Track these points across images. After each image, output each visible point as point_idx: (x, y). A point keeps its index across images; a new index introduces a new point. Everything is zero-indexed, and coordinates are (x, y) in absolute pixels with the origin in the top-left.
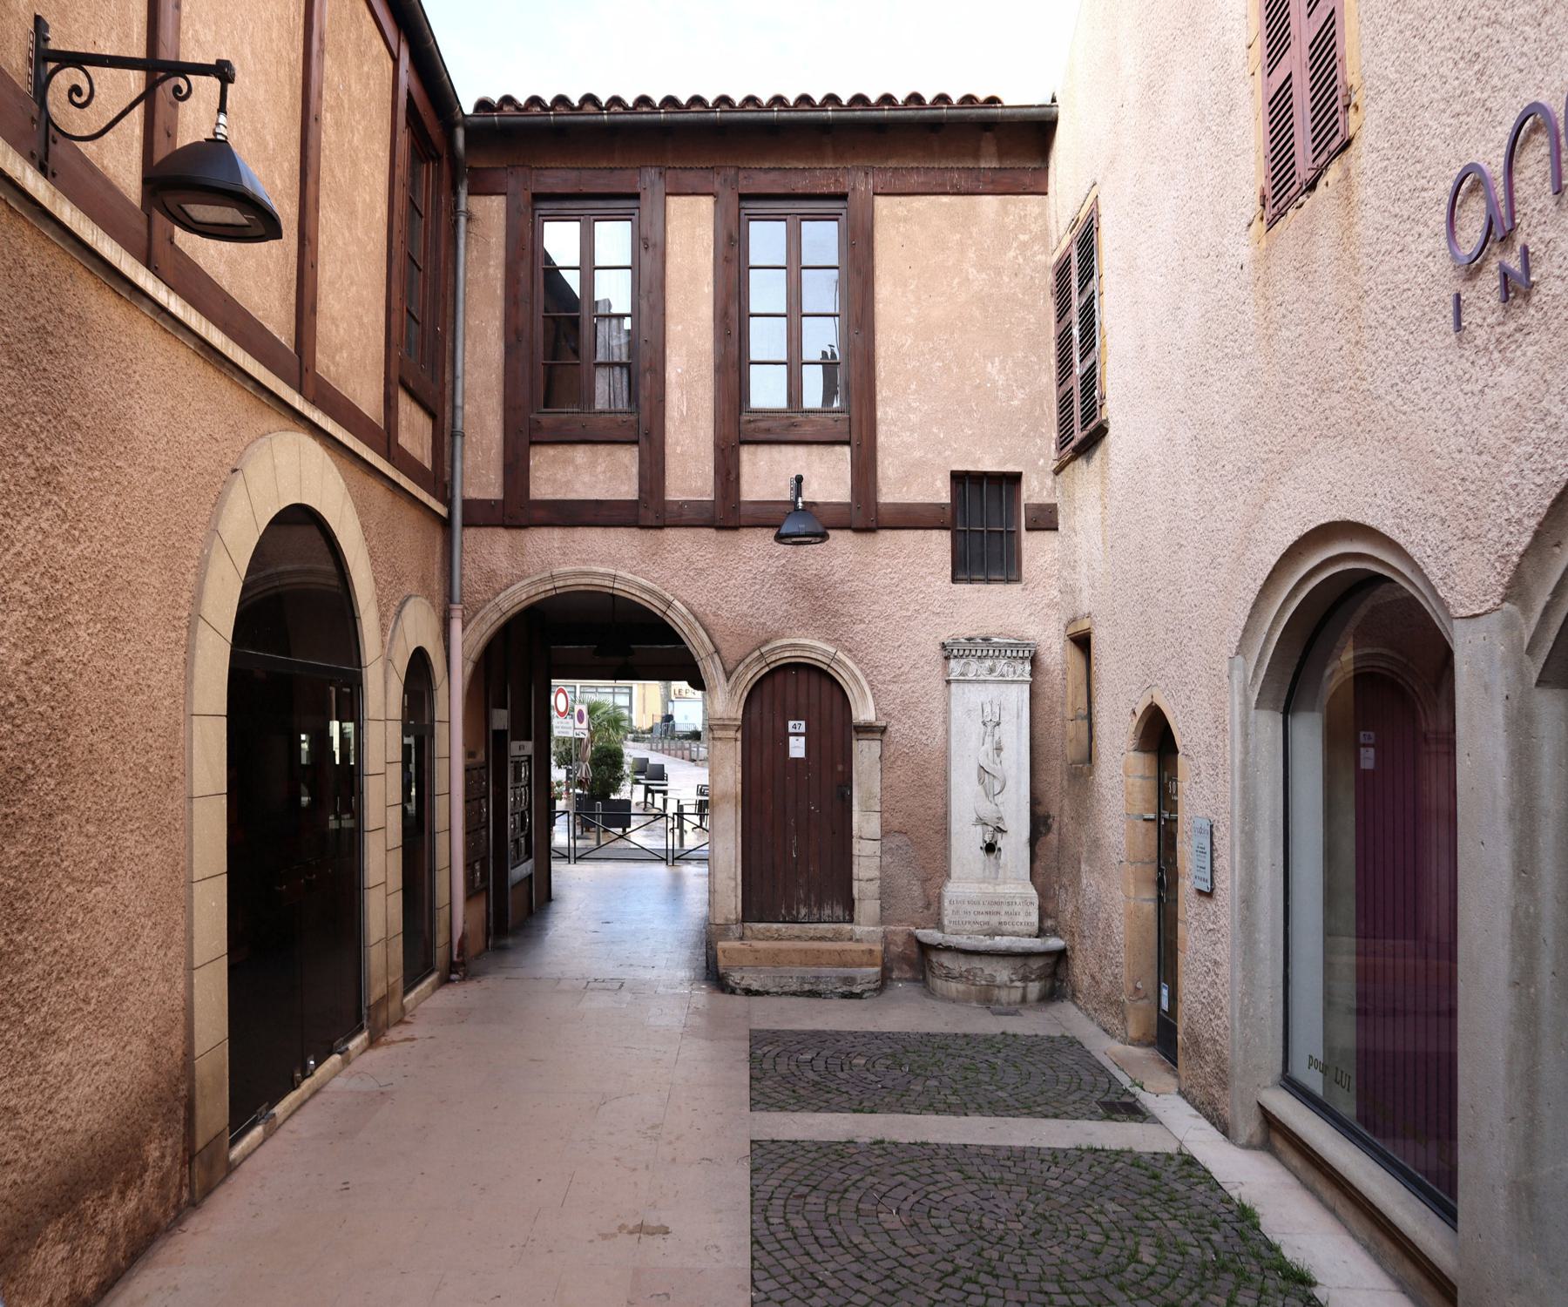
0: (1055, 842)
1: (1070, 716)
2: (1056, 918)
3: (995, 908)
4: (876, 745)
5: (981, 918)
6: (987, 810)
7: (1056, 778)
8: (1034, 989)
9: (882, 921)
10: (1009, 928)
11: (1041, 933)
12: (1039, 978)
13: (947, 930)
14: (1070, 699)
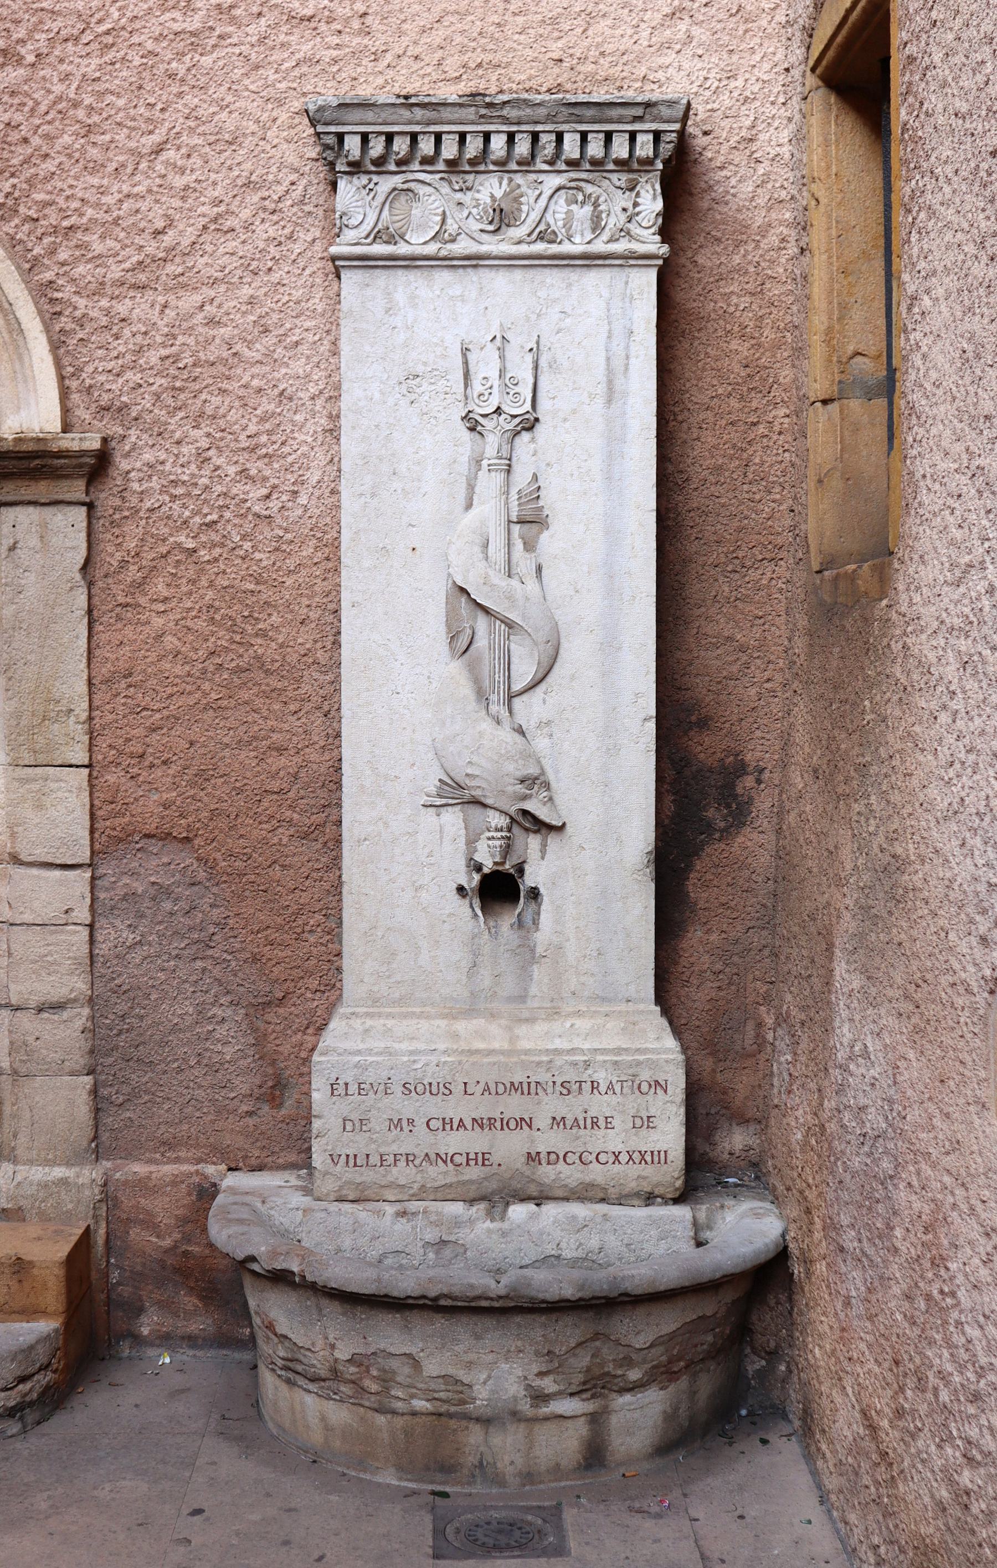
0: (764, 860)
1: (819, 386)
2: (762, 1122)
3: (514, 1106)
4: (68, 526)
5: (454, 1142)
6: (485, 749)
7: (762, 622)
8: (639, 1416)
9: (98, 1147)
10: (570, 1174)
11: (701, 1175)
12: (662, 1374)
13: (326, 1186)
14: (819, 321)
